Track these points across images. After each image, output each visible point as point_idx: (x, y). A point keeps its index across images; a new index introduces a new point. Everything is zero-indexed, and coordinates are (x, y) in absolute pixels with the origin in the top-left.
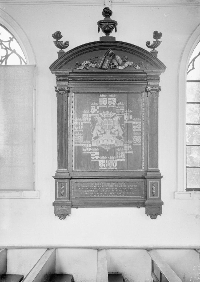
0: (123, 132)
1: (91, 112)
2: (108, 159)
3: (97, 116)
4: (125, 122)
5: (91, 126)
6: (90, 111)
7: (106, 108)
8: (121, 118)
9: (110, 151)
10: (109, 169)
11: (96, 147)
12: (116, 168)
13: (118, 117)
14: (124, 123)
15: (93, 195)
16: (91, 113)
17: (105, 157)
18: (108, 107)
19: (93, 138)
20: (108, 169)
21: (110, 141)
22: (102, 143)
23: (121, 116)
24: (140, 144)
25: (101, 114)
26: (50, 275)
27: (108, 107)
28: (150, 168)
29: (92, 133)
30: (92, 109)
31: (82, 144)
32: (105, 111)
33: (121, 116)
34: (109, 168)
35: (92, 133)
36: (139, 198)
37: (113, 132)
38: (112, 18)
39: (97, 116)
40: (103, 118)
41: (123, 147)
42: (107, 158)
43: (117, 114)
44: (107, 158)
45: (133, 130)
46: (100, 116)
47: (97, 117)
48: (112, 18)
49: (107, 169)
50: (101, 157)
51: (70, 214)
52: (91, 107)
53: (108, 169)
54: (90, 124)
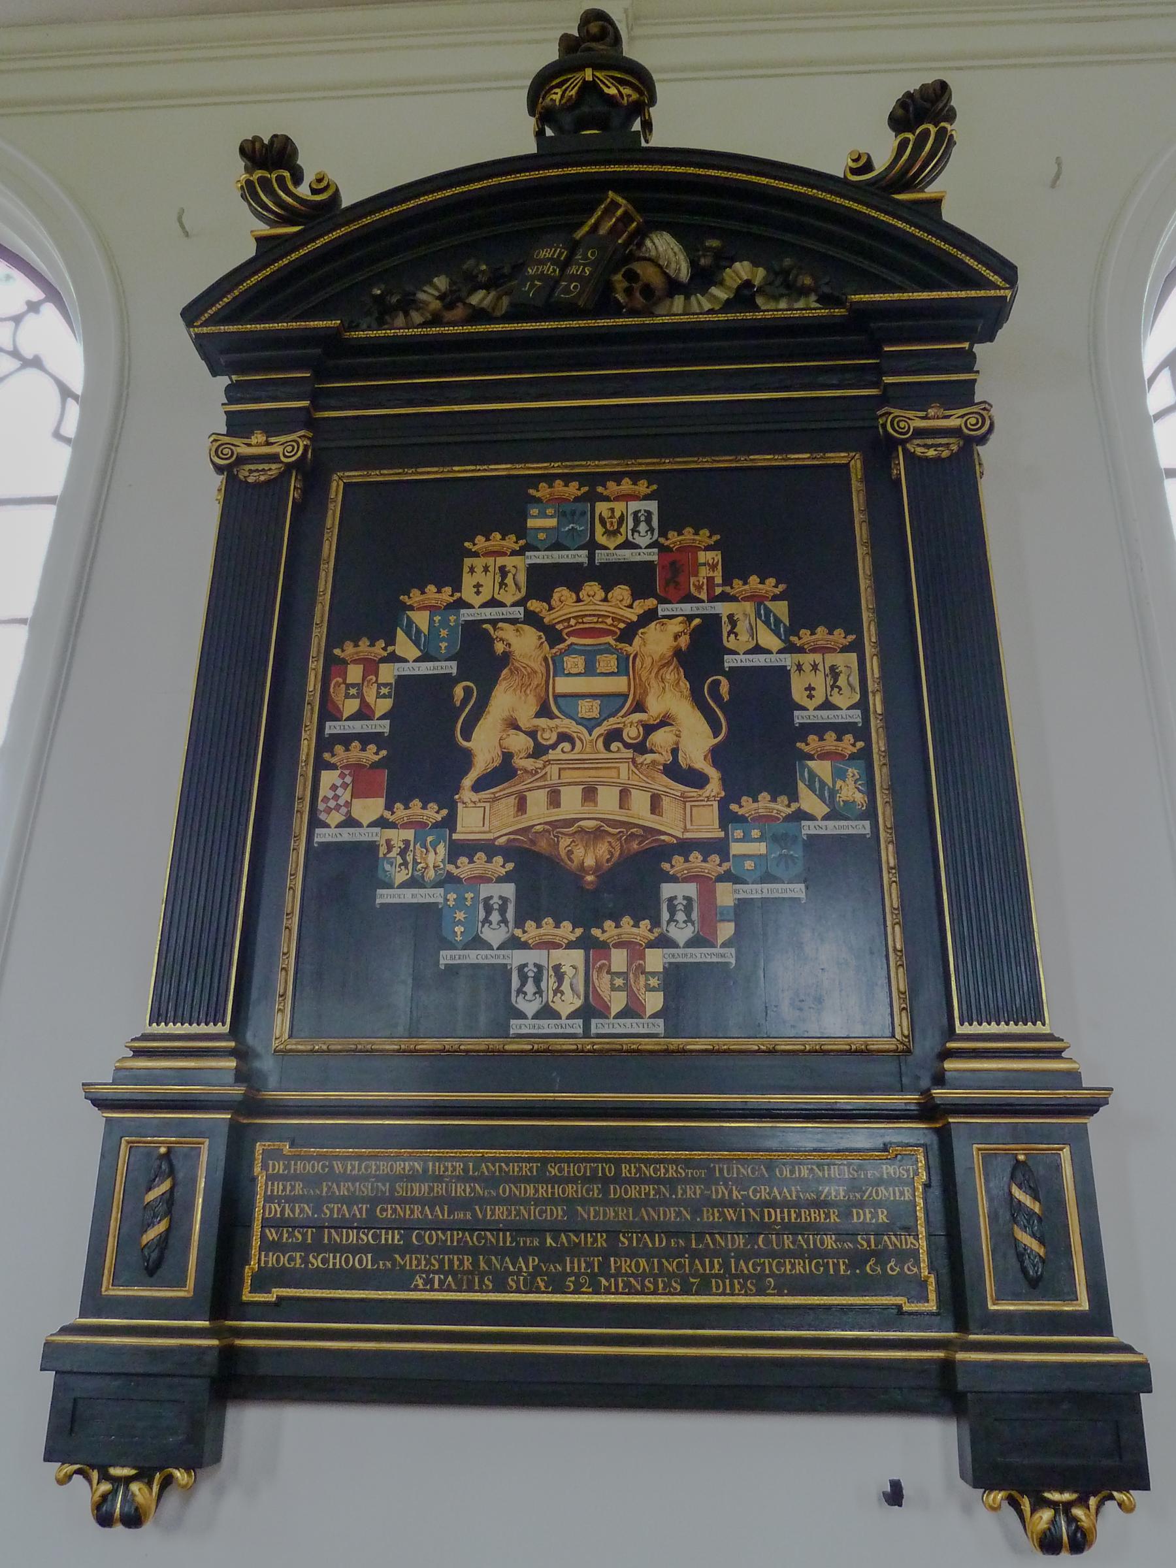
0: (715, 729)
1: (467, 593)
2: (586, 943)
3: (513, 622)
4: (730, 661)
5: (459, 692)
6: (457, 588)
7: (578, 566)
8: (695, 634)
9: (609, 877)
10: (594, 1031)
11: (491, 849)
12: (659, 1026)
13: (675, 626)
14: (719, 669)
15: (441, 1282)
16: (461, 604)
17: (567, 925)
18: (591, 557)
19: (468, 782)
20: (586, 1033)
21: (608, 801)
22: (538, 810)
23: (697, 621)
24: (862, 827)
25: (534, 605)
26: (598, 14)
27: (591, 557)
28: (967, 1018)
29: (468, 738)
30: (468, 581)
31: (377, 830)
32: (576, 588)
33: (697, 621)
34: (597, 1026)
35: (471, 685)
36: (935, 1093)
37: (632, 733)
38: (475, 590)
39: (513, 622)
40: (553, 635)
41: (719, 848)
42: (579, 931)
43: (663, 610)
44: (579, 931)
45: (799, 717)
46: (532, 619)
47: (507, 632)
48: (475, 590)
49: (580, 1031)
50: (530, 925)
51: (193, 1464)
52: (468, 562)
53: (586, 1033)
54: (444, 683)
